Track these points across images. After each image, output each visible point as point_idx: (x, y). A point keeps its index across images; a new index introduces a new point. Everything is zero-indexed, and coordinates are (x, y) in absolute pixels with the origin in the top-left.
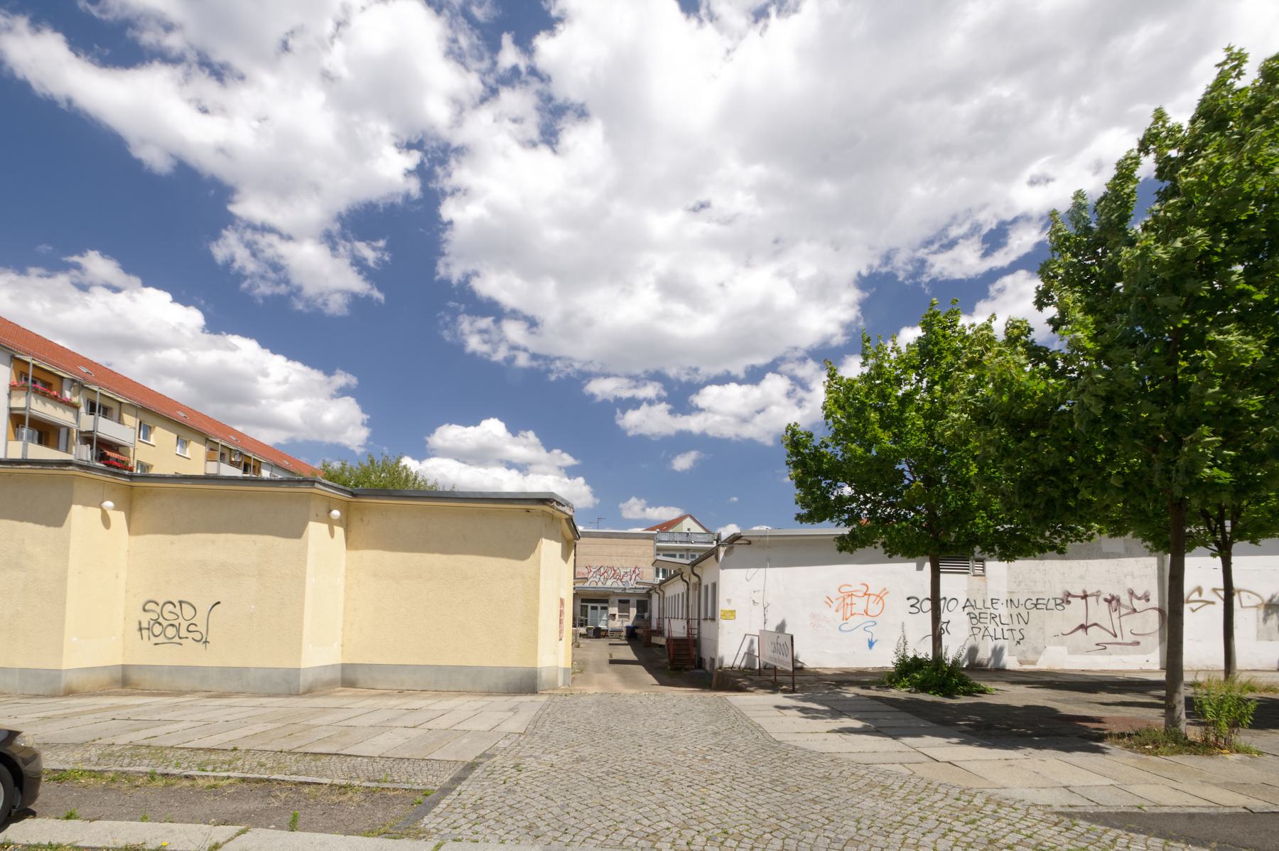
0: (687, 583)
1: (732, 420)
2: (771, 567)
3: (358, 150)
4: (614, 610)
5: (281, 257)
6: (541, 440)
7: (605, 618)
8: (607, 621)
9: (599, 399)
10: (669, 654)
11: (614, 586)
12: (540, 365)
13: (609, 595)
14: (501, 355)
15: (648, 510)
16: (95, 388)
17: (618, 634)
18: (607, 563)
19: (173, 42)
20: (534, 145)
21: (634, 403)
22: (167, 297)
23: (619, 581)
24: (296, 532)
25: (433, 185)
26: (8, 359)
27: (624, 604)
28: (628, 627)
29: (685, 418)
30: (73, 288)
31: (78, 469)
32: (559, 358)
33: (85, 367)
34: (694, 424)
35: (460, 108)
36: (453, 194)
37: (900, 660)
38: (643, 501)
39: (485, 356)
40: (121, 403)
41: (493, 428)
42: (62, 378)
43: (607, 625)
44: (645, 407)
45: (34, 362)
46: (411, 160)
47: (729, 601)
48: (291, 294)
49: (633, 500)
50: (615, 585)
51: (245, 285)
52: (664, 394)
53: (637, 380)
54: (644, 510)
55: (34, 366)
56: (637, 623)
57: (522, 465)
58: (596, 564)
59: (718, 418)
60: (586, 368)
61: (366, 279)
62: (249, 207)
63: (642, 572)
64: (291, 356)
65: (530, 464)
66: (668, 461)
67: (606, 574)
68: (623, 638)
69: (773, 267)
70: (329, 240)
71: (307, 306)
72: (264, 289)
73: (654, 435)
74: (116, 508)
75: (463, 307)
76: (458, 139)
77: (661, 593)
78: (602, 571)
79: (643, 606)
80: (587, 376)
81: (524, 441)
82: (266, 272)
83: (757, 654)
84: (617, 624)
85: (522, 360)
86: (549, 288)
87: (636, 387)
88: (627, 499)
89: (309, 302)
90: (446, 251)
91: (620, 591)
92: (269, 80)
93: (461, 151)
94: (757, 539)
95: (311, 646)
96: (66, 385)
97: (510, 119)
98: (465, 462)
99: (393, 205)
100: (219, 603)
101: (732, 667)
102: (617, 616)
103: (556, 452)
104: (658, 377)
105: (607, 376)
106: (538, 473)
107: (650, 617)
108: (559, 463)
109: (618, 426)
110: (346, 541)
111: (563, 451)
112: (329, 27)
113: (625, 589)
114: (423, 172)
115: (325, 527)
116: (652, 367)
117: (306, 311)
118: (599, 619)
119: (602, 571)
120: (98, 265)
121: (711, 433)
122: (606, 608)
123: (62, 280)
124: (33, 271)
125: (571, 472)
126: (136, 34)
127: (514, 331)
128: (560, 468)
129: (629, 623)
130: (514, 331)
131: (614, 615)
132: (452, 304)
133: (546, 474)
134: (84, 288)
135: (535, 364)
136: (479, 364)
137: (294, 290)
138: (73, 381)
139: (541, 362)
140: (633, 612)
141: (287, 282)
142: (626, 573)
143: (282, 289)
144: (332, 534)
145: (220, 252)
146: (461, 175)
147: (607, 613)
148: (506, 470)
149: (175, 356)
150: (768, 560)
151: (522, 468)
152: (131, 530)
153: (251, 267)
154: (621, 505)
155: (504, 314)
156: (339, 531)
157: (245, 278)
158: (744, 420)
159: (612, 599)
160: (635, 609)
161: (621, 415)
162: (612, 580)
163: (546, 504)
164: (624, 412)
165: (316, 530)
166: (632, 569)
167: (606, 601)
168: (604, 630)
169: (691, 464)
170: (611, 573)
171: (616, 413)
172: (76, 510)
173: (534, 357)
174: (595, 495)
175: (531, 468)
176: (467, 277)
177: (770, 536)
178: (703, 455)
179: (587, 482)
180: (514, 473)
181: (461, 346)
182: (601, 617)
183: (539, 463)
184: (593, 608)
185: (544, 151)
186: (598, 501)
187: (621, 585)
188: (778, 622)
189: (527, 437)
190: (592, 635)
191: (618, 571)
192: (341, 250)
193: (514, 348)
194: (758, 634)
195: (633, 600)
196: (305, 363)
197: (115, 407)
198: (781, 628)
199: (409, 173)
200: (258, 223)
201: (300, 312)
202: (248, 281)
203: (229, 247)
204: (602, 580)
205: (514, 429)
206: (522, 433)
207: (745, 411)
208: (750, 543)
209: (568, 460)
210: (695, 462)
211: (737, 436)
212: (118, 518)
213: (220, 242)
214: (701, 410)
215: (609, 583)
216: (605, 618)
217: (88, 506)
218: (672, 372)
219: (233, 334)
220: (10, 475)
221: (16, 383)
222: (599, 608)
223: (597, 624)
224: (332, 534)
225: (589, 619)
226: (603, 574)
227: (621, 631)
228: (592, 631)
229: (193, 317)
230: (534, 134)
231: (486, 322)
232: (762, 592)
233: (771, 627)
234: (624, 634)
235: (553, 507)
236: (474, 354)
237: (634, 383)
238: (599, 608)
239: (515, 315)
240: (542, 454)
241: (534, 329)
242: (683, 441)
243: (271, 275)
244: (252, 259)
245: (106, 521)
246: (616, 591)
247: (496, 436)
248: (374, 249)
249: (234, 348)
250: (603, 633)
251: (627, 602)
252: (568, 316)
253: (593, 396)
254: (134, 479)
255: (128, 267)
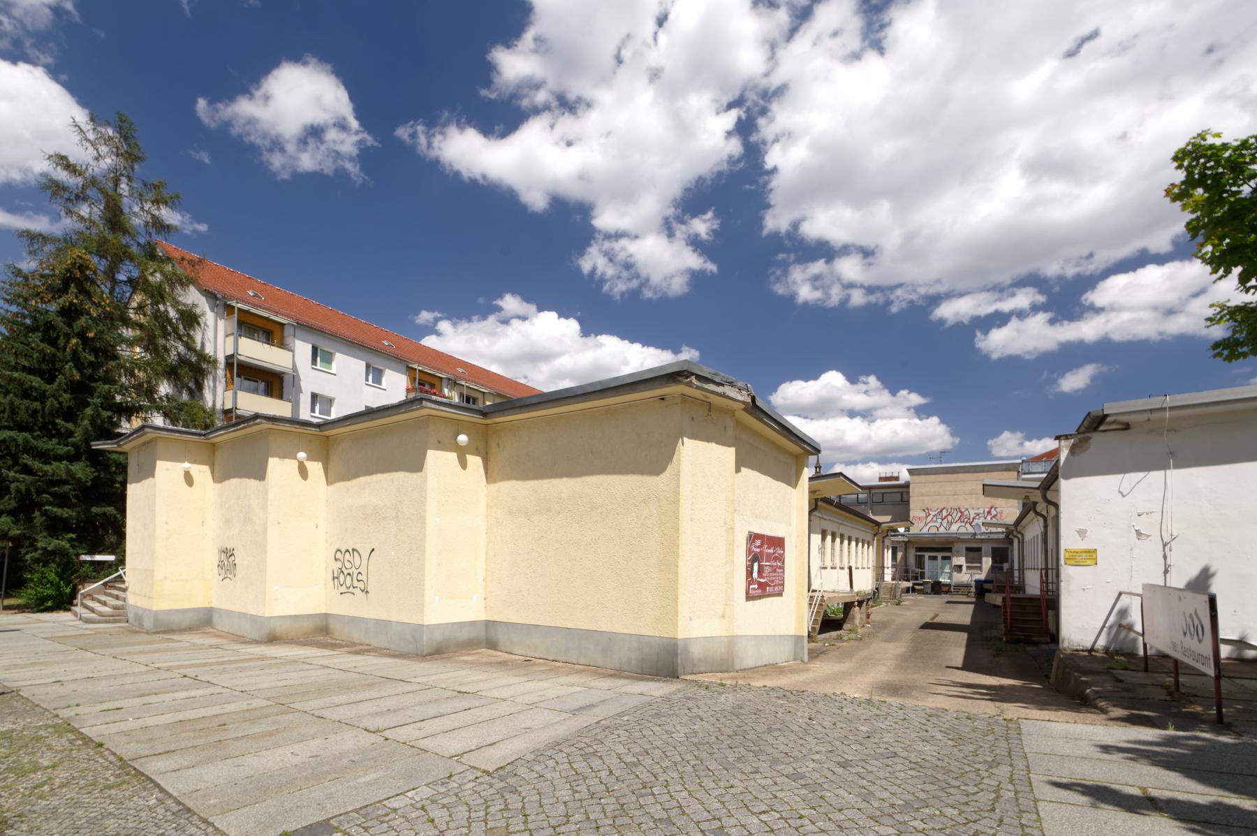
0: (1045, 519)
1: (1146, 315)
2: (1176, 467)
3: (683, 127)
4: (960, 560)
5: (631, 256)
6: (882, 383)
7: (947, 570)
8: (951, 573)
9: (950, 323)
10: (1006, 619)
11: (960, 531)
12: (878, 298)
13: (953, 542)
14: (836, 294)
15: (1027, 444)
16: (463, 383)
17: (966, 590)
18: (952, 503)
19: (541, 97)
20: (856, 56)
21: (1000, 319)
22: (554, 315)
23: (968, 525)
24: (417, 466)
25: (753, 138)
26: (404, 369)
27: (974, 553)
28: (977, 582)
29: (1074, 325)
30: (499, 324)
31: (264, 421)
32: (900, 285)
33: (461, 368)
34: (1088, 330)
35: (772, 47)
36: (776, 140)
37: (61, 308)
38: (1019, 435)
39: (819, 303)
40: (484, 393)
41: (833, 380)
42: (441, 378)
43: (950, 578)
44: (1014, 323)
45: (420, 368)
46: (729, 120)
47: (1082, 533)
48: (641, 285)
49: (1006, 434)
50: (963, 530)
51: (606, 288)
52: (1041, 299)
53: (1001, 290)
54: (1021, 444)
55: (420, 371)
56: (992, 577)
57: (865, 411)
58: (937, 506)
59: (1125, 316)
60: (932, 291)
61: (701, 255)
62: (605, 220)
63: (1001, 513)
64: (646, 343)
65: (875, 409)
66: (1053, 382)
67: (950, 518)
68: (973, 595)
69: (1213, 86)
70: (668, 228)
71: (655, 293)
72: (621, 287)
73: (1028, 353)
74: (310, 458)
75: (792, 257)
76: (775, 81)
77: (1020, 536)
78: (945, 513)
79: (1000, 556)
80: (936, 300)
81: (864, 387)
82: (621, 272)
83: (1138, 628)
84: (965, 577)
85: (858, 298)
86: (883, 211)
87: (1000, 299)
88: (998, 434)
89: (655, 289)
90: (772, 203)
91: (969, 537)
92: (604, 96)
93: (780, 91)
94: (1145, 416)
95: (437, 599)
96: (445, 383)
97: (830, 37)
98: (806, 418)
99: (720, 174)
100: (373, 550)
101: (1092, 650)
102: (964, 568)
103: (904, 393)
104: (1033, 281)
105: (961, 295)
106: (883, 418)
107: (1012, 568)
108: (906, 404)
109: (978, 351)
110: (486, 473)
111: (911, 391)
112: (651, 26)
113: (975, 534)
114: (744, 129)
115: (453, 456)
116: (1024, 269)
117: (655, 297)
118: (939, 571)
119: (945, 513)
120: (510, 303)
121: (1117, 337)
122: (949, 558)
123: (492, 319)
124: (475, 318)
125: (921, 412)
126: (519, 102)
127: (849, 268)
128: (909, 409)
129: (982, 576)
130: (849, 268)
131: (960, 567)
132: (781, 256)
133: (892, 418)
134: (506, 322)
135: (872, 298)
136: (813, 311)
137: (643, 281)
138: (449, 379)
139: (879, 294)
140: (987, 562)
141: (637, 276)
142: (978, 515)
143: (634, 284)
144: (463, 464)
145: (586, 265)
146: (782, 117)
147: (951, 564)
148: (849, 419)
149: (564, 362)
150: (1172, 454)
151: (866, 414)
152: (330, 480)
153: (610, 271)
154: (990, 442)
155: (836, 252)
156: (475, 461)
157: (606, 281)
158: (1170, 312)
159: (956, 547)
160: (990, 559)
161: (983, 337)
162: (959, 524)
163: (680, 382)
164: (986, 331)
165: (439, 462)
166: (987, 510)
167: (949, 550)
168: (946, 585)
169: (1088, 381)
170: (957, 515)
171: (976, 336)
172: (273, 462)
173: (870, 290)
174: (953, 435)
175: (879, 413)
176: (796, 225)
177: (1171, 408)
178: (1105, 368)
179: (943, 421)
180: (857, 421)
181: (792, 297)
182: (943, 568)
183: (884, 407)
184: (931, 558)
185: (871, 58)
186: (957, 440)
187: (970, 530)
188: (1194, 572)
189: (866, 383)
190: (929, 591)
191: (966, 513)
192: (678, 234)
193: (851, 285)
194: (1140, 591)
195: (986, 548)
196: (657, 347)
197: (480, 396)
198: (1201, 582)
199: (729, 134)
200: (613, 232)
201: (650, 300)
202: (609, 283)
203: (593, 260)
204: (945, 525)
205: (852, 378)
206: (863, 378)
207: (1170, 298)
208: (1127, 427)
209: (916, 399)
210: (1094, 379)
211: (1160, 334)
212: (315, 468)
213: (586, 257)
214: (1099, 310)
215: (954, 528)
216: (947, 570)
217: (284, 458)
218: (1052, 269)
219: (601, 335)
220: (245, 438)
221: (410, 387)
222: (939, 558)
223: (937, 577)
224: (463, 464)
225: (926, 570)
226: (946, 517)
227: (968, 586)
228: (930, 585)
229: (572, 326)
230: (855, 43)
231: (818, 267)
232: (1157, 516)
233: (1178, 580)
234: (973, 590)
235: (690, 384)
236: (806, 304)
237: (997, 295)
238: (939, 558)
239: (845, 250)
240: (885, 397)
241: (870, 259)
242: (1071, 355)
243: (625, 274)
244: (610, 264)
245: (303, 472)
246: (961, 537)
247: (835, 387)
248: (705, 221)
249: (601, 345)
250: (945, 589)
251: (979, 550)
252: (909, 238)
253: (942, 321)
254: (323, 428)
255: (527, 299)
